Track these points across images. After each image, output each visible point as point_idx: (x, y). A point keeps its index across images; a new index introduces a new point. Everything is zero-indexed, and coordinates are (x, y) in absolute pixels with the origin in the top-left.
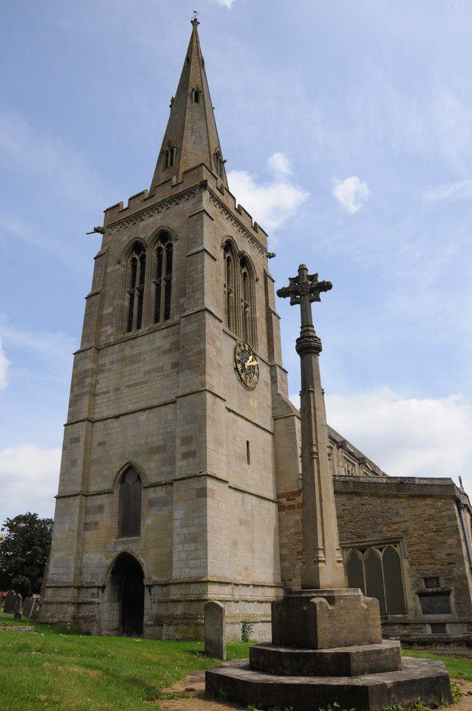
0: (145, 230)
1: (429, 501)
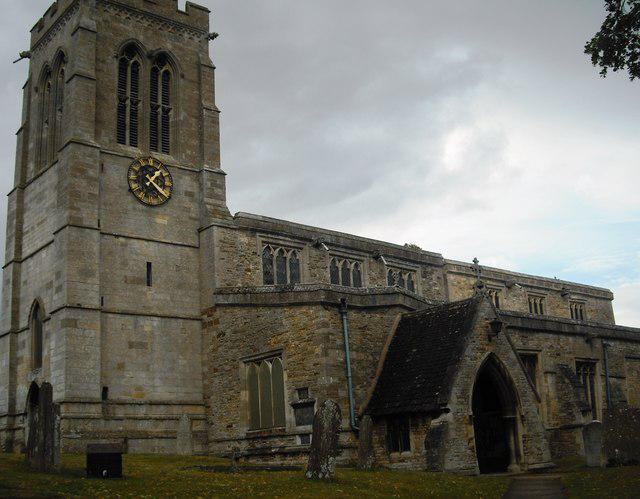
0: (49, 54)
1: (304, 309)
